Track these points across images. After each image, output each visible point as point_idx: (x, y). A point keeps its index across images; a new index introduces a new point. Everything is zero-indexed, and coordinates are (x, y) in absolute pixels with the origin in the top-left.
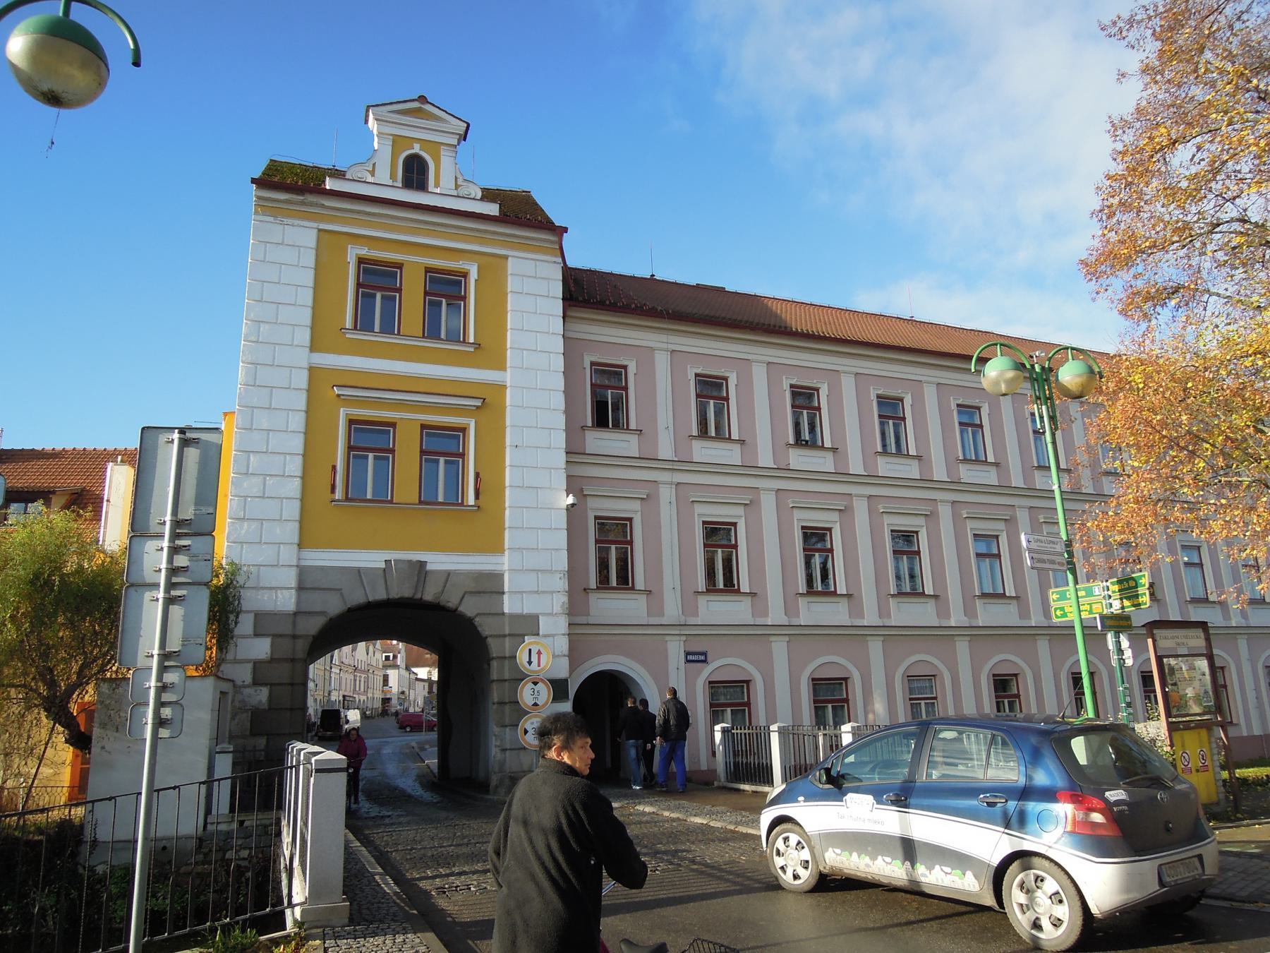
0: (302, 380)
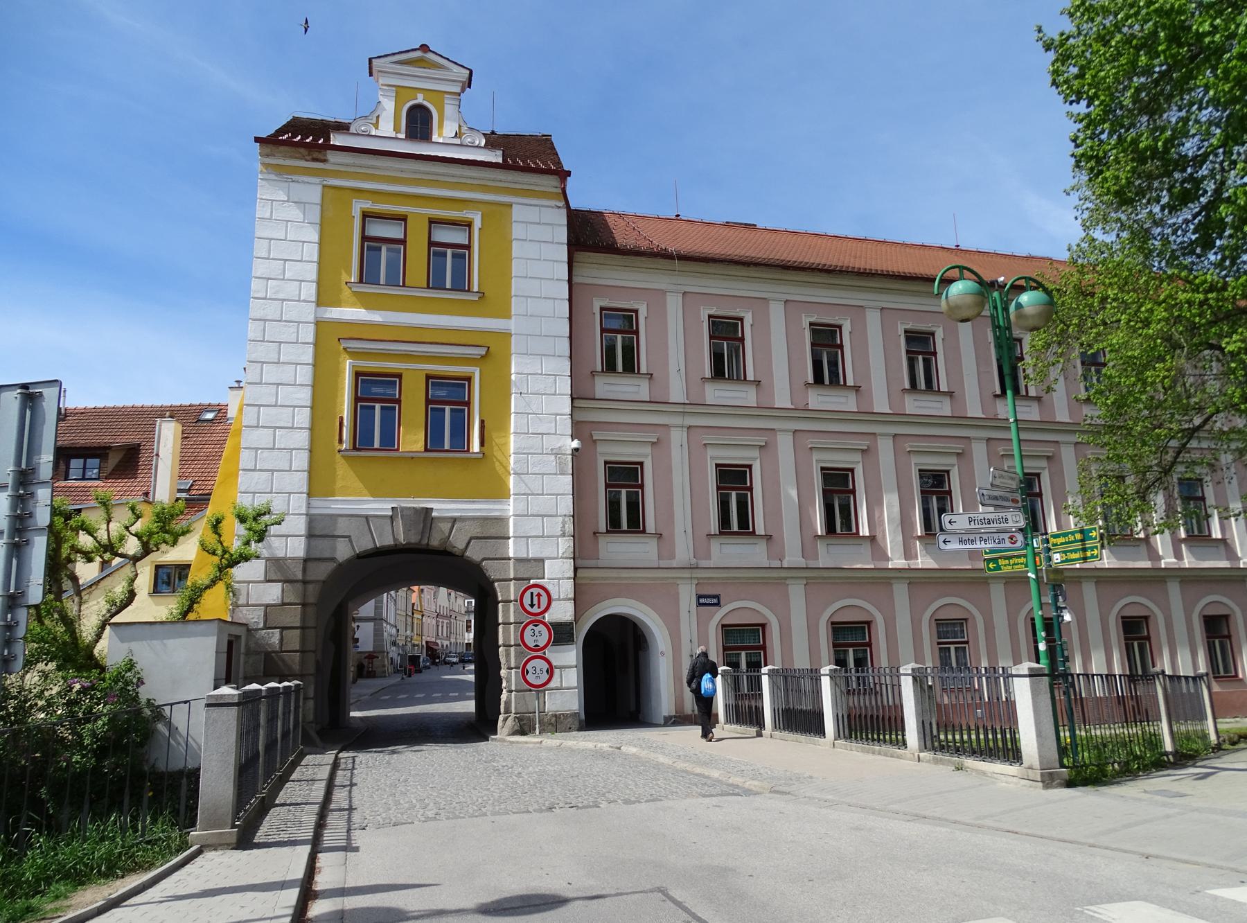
0: (308, 334)
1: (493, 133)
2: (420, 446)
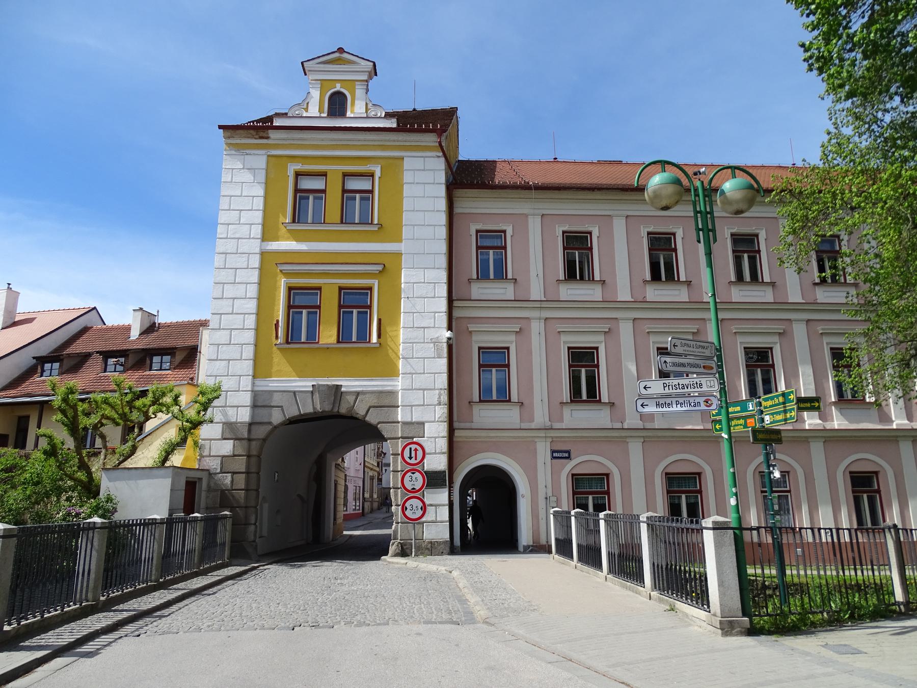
0: (255, 261)
1: (414, 110)
2: (333, 339)
